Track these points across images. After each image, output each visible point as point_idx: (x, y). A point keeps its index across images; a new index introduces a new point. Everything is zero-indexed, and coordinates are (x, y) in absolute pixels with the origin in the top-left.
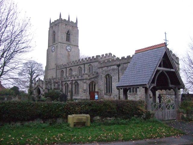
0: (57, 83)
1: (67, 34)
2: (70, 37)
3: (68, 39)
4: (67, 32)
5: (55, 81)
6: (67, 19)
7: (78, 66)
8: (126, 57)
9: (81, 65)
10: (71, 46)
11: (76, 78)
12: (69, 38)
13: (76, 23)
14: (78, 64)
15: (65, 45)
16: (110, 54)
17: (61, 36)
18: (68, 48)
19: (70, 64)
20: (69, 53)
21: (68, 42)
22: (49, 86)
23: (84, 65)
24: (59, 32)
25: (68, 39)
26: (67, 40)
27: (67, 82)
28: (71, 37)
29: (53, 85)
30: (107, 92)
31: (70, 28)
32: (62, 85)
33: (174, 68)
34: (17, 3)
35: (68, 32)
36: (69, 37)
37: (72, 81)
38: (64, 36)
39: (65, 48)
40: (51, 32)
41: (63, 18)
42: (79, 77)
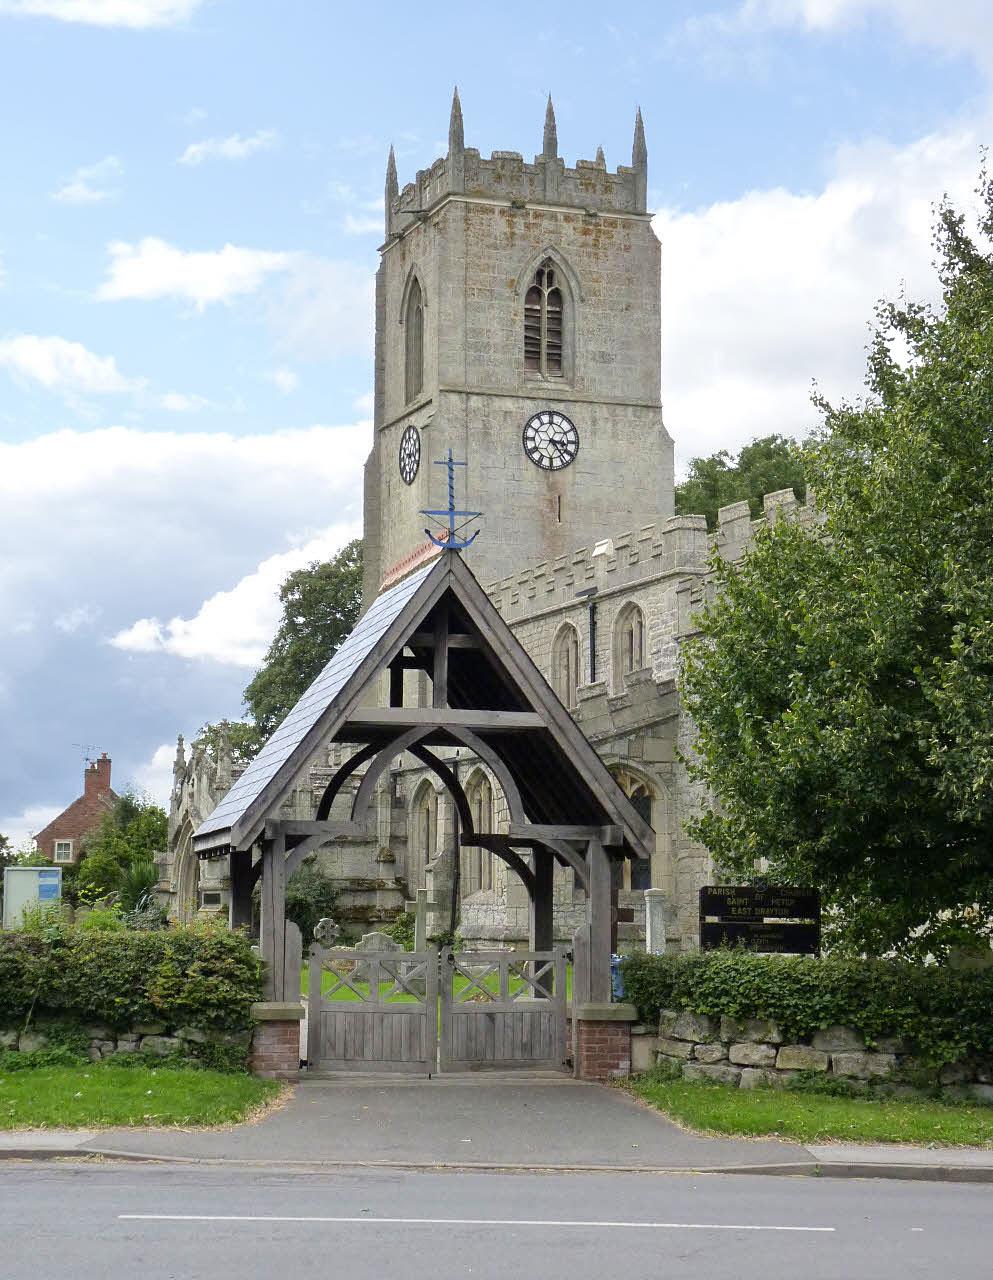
1: (534, 293)
2: (568, 325)
3: (545, 344)
4: (539, 274)
6: (531, 153)
8: (414, 182)
10: (579, 413)
12: (557, 333)
13: (634, 179)
15: (509, 404)
16: (218, 253)
17: (480, 324)
18: (544, 434)
20: (552, 487)
21: (551, 384)
23: (593, 610)
25: (545, 344)
26: (532, 356)
28: (582, 324)
31: (568, 229)
33: (444, 589)
35: (545, 273)
36: (557, 318)
38: (504, 323)
39: (510, 434)
40: (396, 290)
41: (484, 141)
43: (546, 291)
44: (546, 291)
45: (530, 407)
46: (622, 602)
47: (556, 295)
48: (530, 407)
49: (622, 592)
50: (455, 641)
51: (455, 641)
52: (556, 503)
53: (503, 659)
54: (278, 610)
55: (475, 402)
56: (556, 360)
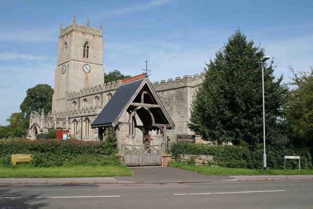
0: (61, 119)
1: (85, 46)
3: (86, 54)
4: (86, 43)
5: (58, 117)
7: (95, 96)
9: (98, 93)
10: (91, 65)
11: (87, 114)
14: (95, 92)
19: (84, 92)
22: (50, 124)
24: (72, 44)
25: (86, 54)
26: (84, 56)
27: (111, 92)
29: (55, 122)
30: (130, 133)
32: (69, 123)
34: (282, 77)
36: (88, 50)
37: (82, 117)
42: (91, 111)
43: (86, 46)
44: (86, 46)
45: (84, 63)
46: (84, 98)
47: (88, 47)
48: (84, 63)
49: (74, 118)
50: (145, 92)
51: (145, 92)
52: (87, 79)
53: (154, 96)
54: (26, 94)
55: (76, 62)
56: (87, 57)
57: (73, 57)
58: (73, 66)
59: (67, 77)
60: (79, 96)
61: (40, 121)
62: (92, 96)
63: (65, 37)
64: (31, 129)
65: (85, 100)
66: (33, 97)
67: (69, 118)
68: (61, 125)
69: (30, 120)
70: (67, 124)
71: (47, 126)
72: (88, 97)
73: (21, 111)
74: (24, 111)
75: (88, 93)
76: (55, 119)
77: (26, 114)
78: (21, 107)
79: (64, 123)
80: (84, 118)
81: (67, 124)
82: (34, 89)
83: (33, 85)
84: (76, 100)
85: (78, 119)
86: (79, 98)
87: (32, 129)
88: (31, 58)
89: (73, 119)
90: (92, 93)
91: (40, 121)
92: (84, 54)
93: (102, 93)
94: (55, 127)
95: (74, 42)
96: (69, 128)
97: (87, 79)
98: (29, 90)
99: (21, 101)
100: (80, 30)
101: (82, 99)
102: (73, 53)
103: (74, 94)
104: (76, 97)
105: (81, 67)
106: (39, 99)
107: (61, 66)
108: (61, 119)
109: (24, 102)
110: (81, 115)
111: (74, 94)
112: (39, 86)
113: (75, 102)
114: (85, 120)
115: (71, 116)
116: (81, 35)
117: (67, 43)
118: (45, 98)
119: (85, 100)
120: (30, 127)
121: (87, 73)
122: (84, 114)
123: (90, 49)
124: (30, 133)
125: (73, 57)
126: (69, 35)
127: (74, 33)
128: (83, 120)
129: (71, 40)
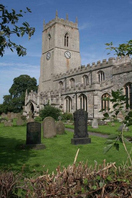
1: (65, 37)
3: (66, 43)
4: (66, 35)
7: (83, 75)
11: (82, 90)
22: (46, 100)
25: (66, 43)
26: (65, 44)
27: (102, 70)
29: (50, 99)
36: (68, 40)
37: (76, 93)
44: (66, 36)
45: (65, 51)
48: (65, 51)
52: (68, 63)
55: (59, 49)
56: (67, 46)
57: (56, 45)
58: (57, 53)
59: (52, 62)
60: (65, 76)
61: (36, 98)
62: (79, 75)
63: (48, 30)
64: (26, 105)
65: (73, 79)
66: (18, 84)
67: (61, 95)
68: (54, 101)
69: (26, 98)
70: (60, 101)
71: (43, 103)
72: (75, 76)
73: (10, 94)
74: (11, 94)
75: (75, 73)
76: (49, 95)
77: (13, 96)
78: (10, 91)
79: (58, 100)
80: (78, 95)
81: (60, 101)
82: (18, 78)
83: (17, 75)
84: (63, 80)
85: (71, 96)
86: (66, 78)
87: (28, 106)
88: (5, 64)
89: (65, 96)
90: (79, 72)
91: (36, 98)
92: (65, 43)
93: (91, 72)
94: (50, 104)
95: (57, 33)
96: (61, 104)
97: (68, 63)
98: (15, 79)
99: (10, 87)
100: (62, 23)
101: (68, 79)
102: (56, 42)
103: (61, 76)
104: (63, 77)
105: (63, 53)
106: (23, 85)
107: (45, 54)
108: (55, 97)
109: (12, 87)
110: (75, 91)
111: (61, 76)
112: (21, 76)
113: (61, 83)
114: (79, 96)
115: (64, 93)
116: (62, 27)
117: (51, 34)
118: (26, 85)
119: (73, 79)
120: (26, 104)
121: (68, 59)
122: (78, 91)
123: (69, 39)
124: (26, 109)
125: (56, 45)
126: (52, 28)
127: (57, 25)
128: (78, 96)
129: (54, 31)
